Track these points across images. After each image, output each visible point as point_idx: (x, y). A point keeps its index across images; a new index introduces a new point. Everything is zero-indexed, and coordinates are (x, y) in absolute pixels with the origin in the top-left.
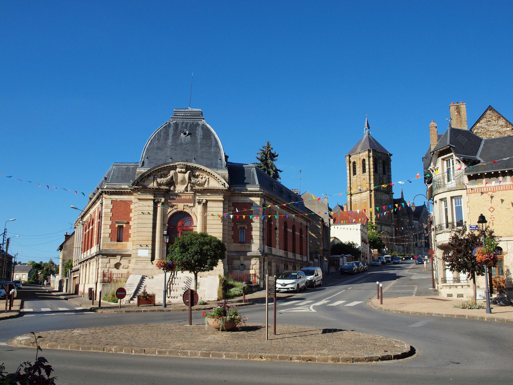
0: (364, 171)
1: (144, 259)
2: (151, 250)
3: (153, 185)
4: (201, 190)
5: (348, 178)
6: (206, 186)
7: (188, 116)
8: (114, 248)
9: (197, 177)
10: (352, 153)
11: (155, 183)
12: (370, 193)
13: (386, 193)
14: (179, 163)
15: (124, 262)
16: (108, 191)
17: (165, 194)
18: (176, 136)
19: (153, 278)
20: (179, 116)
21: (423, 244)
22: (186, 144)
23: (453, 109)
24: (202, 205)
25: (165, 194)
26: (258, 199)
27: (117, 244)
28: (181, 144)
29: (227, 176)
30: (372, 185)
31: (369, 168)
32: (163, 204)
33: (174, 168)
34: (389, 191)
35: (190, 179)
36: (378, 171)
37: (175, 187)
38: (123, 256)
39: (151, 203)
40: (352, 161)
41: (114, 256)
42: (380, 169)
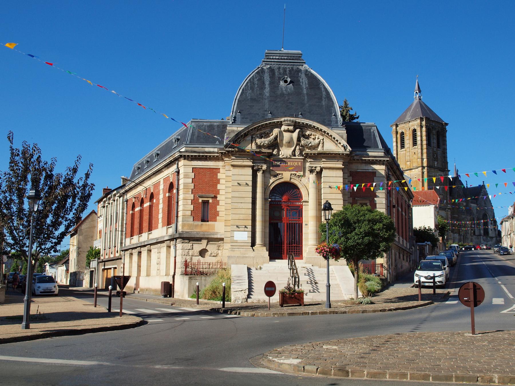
0: (415, 143)
1: (243, 244)
2: (251, 232)
3: (251, 147)
4: (314, 154)
6: (320, 149)
7: (284, 59)
8: (198, 230)
9: (308, 137)
10: (400, 121)
11: (253, 144)
12: (422, 169)
13: (440, 170)
14: (286, 118)
15: (212, 248)
16: (188, 156)
17: (266, 160)
18: (274, 85)
19: (261, 268)
20: (273, 59)
21: (482, 232)
22: (289, 94)
24: (315, 173)
25: (266, 160)
26: (383, 167)
27: (202, 225)
28: (282, 95)
29: (345, 136)
30: (425, 160)
31: (422, 140)
32: (264, 172)
33: (279, 125)
34: (444, 169)
35: (299, 140)
36: (432, 144)
37: (279, 151)
38: (210, 240)
39: (250, 171)
40: (400, 131)
41: (199, 240)
42: (434, 141)
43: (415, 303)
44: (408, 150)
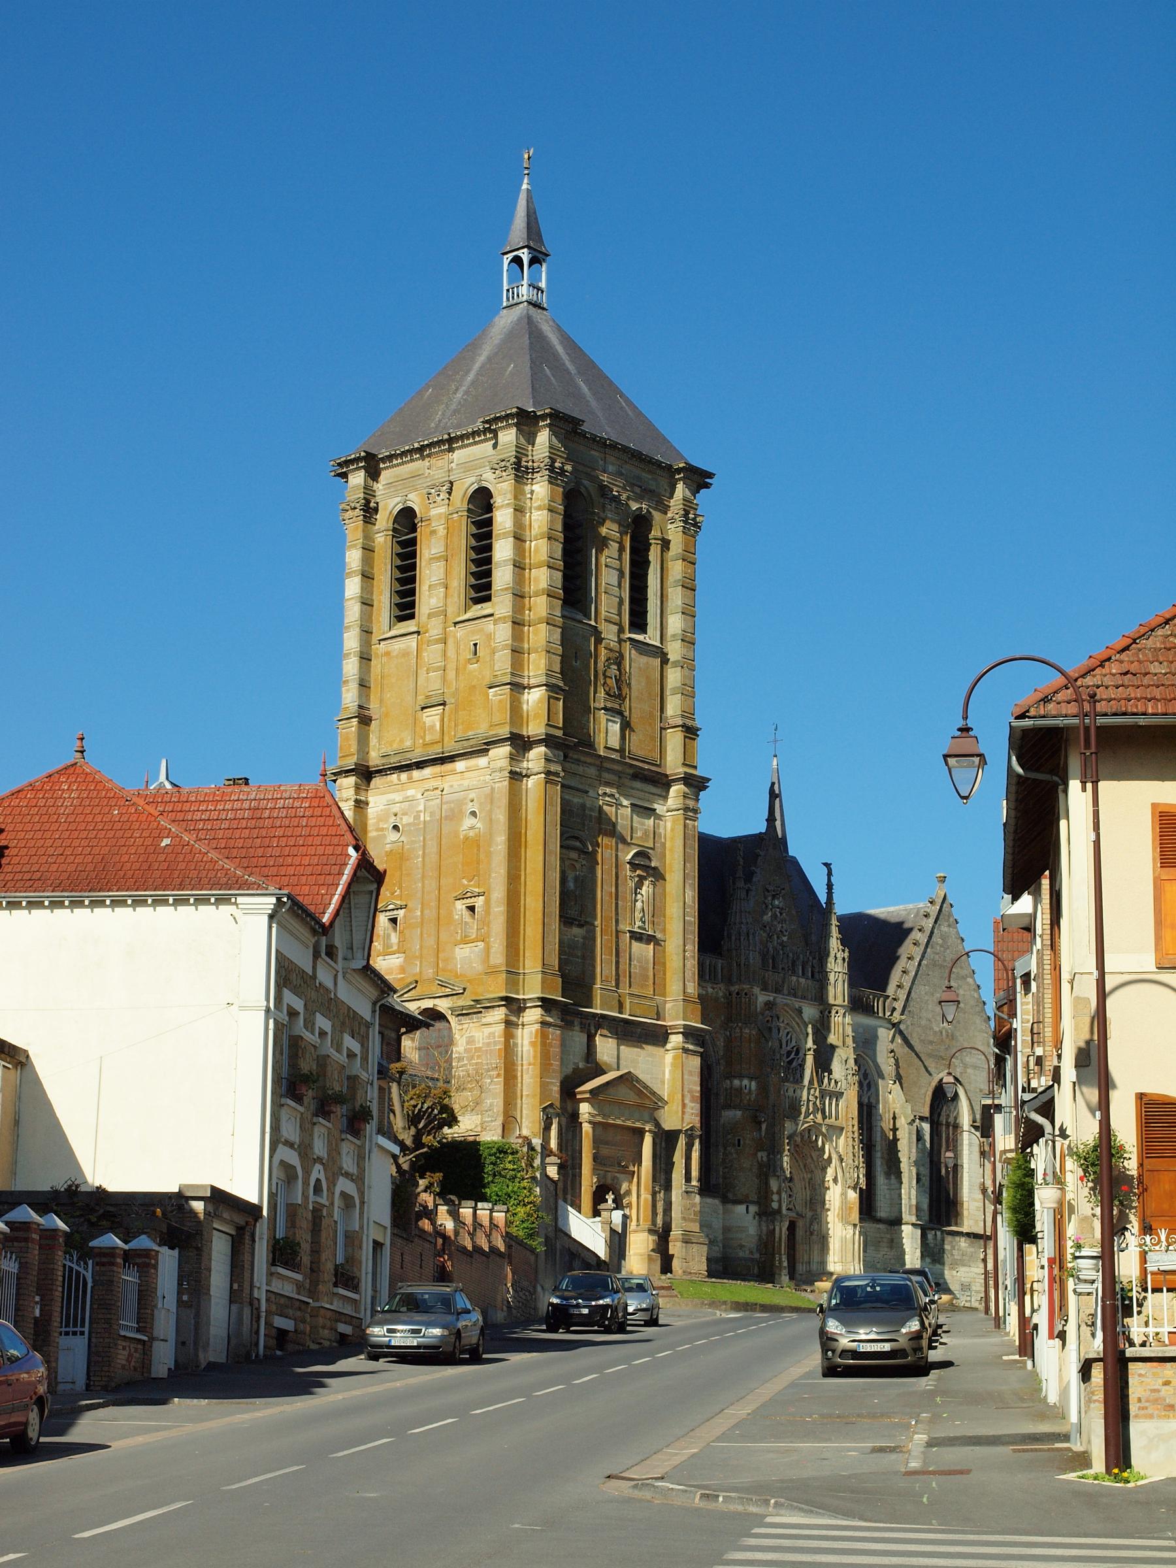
0: (481, 589)
5: (351, 641)
23: (576, 1311)
43: (660, 1210)
44: (434, 629)
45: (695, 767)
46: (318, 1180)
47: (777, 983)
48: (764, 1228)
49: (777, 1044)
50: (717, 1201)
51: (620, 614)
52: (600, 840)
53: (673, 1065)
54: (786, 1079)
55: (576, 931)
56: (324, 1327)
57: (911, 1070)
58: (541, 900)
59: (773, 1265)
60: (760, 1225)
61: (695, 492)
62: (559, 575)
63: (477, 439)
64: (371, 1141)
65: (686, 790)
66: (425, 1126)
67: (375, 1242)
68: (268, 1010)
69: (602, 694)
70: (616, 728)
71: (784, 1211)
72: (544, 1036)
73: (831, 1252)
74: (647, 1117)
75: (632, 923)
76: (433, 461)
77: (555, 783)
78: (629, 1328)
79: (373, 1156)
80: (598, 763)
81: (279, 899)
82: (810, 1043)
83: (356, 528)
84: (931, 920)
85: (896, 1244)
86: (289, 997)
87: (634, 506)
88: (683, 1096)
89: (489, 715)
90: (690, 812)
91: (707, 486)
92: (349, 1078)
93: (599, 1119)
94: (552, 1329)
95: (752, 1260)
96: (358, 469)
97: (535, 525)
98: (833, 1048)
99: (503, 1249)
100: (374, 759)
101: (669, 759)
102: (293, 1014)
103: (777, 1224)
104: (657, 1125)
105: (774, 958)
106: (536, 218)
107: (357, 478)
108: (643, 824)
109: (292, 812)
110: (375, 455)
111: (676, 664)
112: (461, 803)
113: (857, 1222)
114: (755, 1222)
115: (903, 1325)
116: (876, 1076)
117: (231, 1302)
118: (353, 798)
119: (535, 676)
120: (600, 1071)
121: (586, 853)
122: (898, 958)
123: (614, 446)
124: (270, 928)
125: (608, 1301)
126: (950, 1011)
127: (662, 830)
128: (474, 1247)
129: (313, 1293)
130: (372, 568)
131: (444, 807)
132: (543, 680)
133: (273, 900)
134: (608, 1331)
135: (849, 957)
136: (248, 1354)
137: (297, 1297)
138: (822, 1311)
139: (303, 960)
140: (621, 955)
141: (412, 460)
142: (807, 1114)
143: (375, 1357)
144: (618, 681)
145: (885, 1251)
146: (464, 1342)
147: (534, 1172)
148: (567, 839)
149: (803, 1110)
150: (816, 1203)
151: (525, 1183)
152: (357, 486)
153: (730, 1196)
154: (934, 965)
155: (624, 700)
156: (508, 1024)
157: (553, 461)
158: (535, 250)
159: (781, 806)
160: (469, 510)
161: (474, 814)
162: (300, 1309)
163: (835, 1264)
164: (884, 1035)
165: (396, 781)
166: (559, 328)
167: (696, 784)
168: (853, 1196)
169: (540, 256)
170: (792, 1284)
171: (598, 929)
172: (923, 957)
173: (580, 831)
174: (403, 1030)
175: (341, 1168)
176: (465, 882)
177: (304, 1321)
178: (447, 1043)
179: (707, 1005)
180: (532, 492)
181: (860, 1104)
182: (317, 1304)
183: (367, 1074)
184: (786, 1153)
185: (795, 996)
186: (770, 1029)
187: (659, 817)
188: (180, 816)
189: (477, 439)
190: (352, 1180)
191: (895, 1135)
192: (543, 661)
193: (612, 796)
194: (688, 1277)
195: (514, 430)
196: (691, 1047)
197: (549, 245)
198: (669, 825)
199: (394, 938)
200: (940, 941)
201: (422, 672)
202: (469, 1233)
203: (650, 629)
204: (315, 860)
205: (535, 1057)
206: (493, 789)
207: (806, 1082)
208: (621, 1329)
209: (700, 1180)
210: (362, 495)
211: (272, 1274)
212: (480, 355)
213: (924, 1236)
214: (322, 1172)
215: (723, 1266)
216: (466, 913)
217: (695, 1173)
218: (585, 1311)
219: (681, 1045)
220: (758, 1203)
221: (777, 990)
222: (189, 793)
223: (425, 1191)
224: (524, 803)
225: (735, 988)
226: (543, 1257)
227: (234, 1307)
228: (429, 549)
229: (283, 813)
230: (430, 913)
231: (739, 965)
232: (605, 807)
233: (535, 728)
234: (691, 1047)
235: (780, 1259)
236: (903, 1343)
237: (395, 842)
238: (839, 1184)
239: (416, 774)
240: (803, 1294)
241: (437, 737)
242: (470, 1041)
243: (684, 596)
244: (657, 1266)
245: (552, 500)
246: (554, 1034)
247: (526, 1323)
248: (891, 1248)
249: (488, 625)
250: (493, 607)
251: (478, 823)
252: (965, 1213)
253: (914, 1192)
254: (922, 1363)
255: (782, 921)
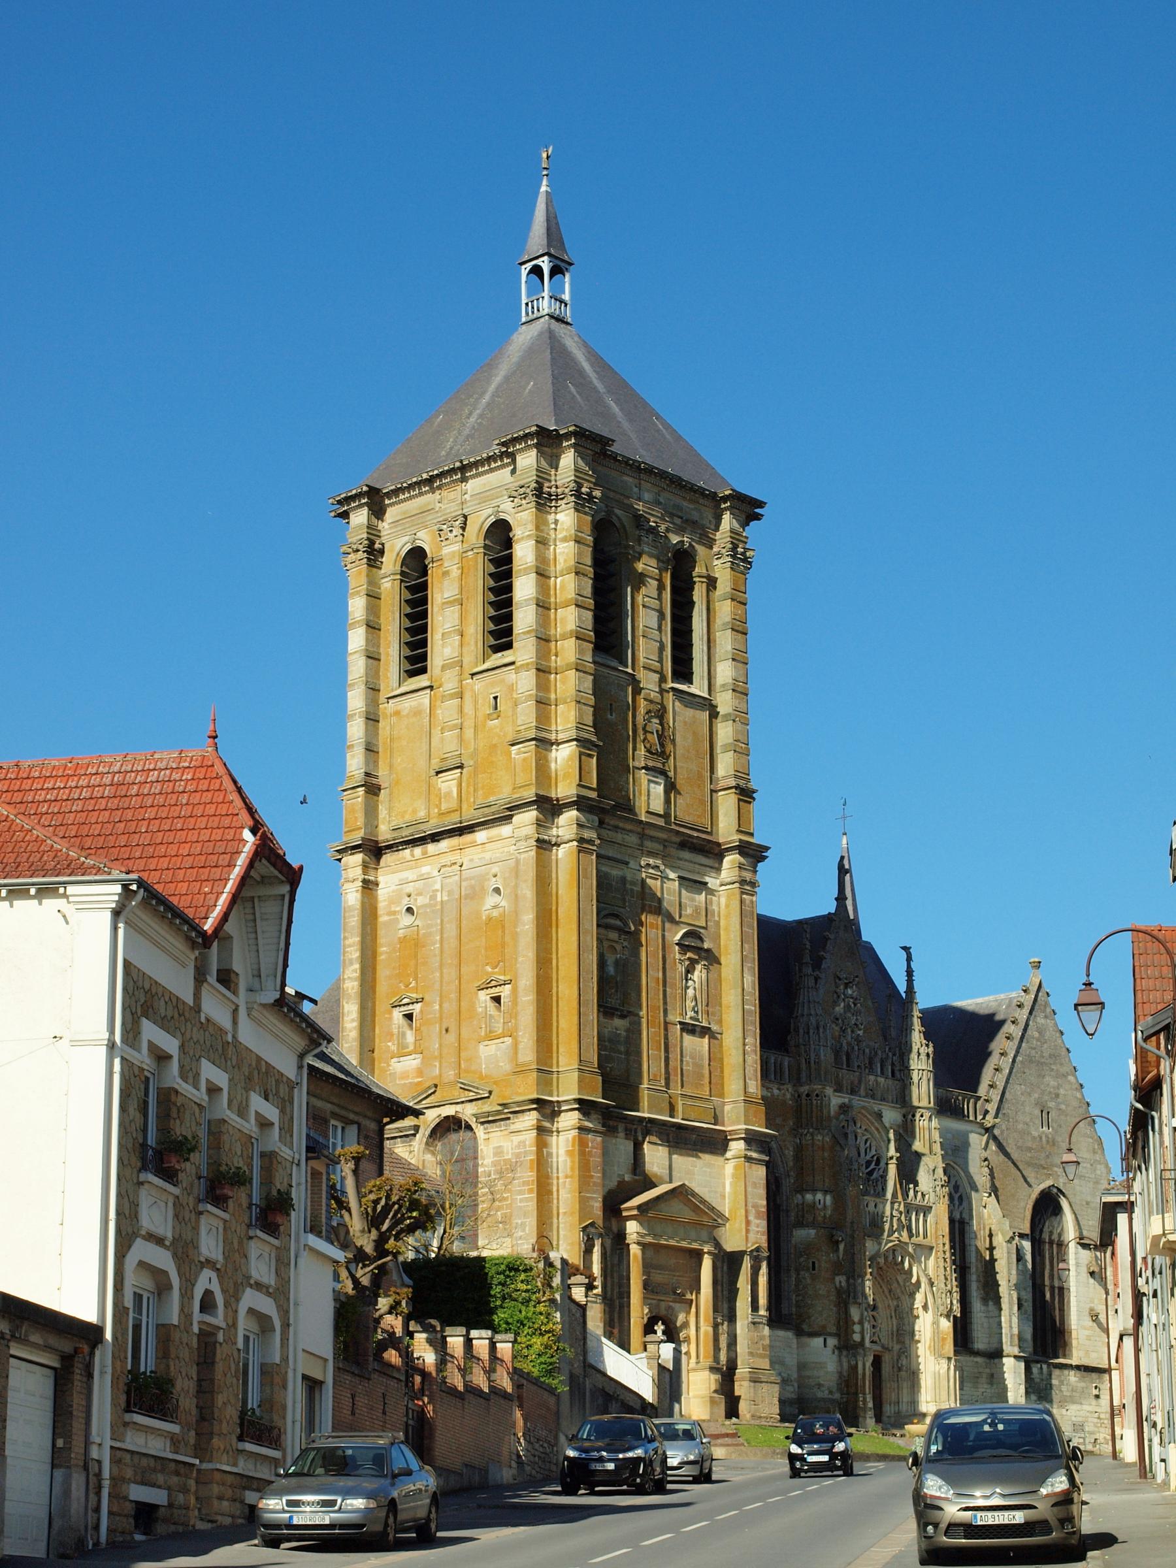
0: (501, 635)
5: (356, 700)
23: (599, 1467)
40: (396, 546)
44: (449, 682)
45: (752, 835)
46: (208, 1294)
47: (852, 1083)
48: (845, 1365)
49: (854, 1153)
50: (790, 1334)
51: (661, 661)
52: (643, 918)
53: (734, 1176)
54: (865, 1193)
55: (618, 1022)
56: (220, 1498)
57: (1009, 1181)
58: (576, 987)
59: (856, 1407)
60: (840, 1361)
61: (745, 524)
62: (589, 616)
63: (493, 465)
64: (297, 1241)
65: (742, 860)
66: (390, 1229)
67: (305, 1377)
68: (111, 1046)
69: (641, 751)
70: (659, 790)
71: (867, 1344)
72: (582, 1144)
73: (923, 1390)
74: (704, 1235)
75: (683, 1013)
76: (445, 493)
77: (590, 852)
78: (669, 1486)
79: (301, 1261)
80: (639, 830)
81: (125, 887)
82: (892, 1151)
83: (360, 573)
84: (1026, 1011)
85: (996, 1380)
86: (150, 1031)
87: (675, 539)
88: (746, 1211)
89: (513, 777)
90: (747, 886)
91: (758, 517)
92: (263, 1155)
93: (649, 1239)
94: (570, 1491)
95: (833, 1400)
96: (361, 506)
97: (561, 559)
98: (918, 1156)
99: (509, 1390)
100: (384, 833)
101: (721, 825)
102: (162, 1058)
103: (860, 1359)
104: (717, 1245)
105: (848, 1055)
106: (557, 224)
107: (360, 517)
108: (693, 900)
109: (168, 787)
110: (378, 491)
111: (727, 717)
112: (482, 879)
113: (951, 1354)
114: (835, 1357)
115: (1042, 1482)
116: (968, 1190)
117: (53, 1466)
118: (361, 877)
119: (565, 730)
120: (650, 1184)
121: (629, 933)
122: (990, 1054)
123: (650, 471)
124: (115, 929)
125: (639, 1452)
126: (1090, 1015)
127: (715, 907)
128: (465, 1386)
129: (202, 1450)
130: (379, 617)
131: (464, 884)
132: (573, 734)
133: (118, 888)
134: (640, 1491)
135: (935, 1052)
136: (81, 1542)
137: (171, 1456)
138: (916, 1462)
139: (176, 980)
140: (671, 1049)
141: (421, 494)
142: (891, 1232)
143: (273, 1542)
144: (660, 737)
145: (984, 1387)
146: (401, 1517)
147: (553, 1293)
148: (606, 916)
149: (887, 1226)
150: (904, 1334)
151: (541, 1308)
152: (360, 526)
153: (805, 1327)
154: (1031, 1061)
155: (668, 758)
156: (541, 1130)
157: (580, 486)
158: (557, 258)
159: (852, 883)
160: (486, 547)
161: (497, 891)
162: (177, 1474)
163: (929, 1403)
164: (977, 1141)
165: (409, 857)
166: (586, 345)
167: (754, 853)
168: (946, 1325)
169: (562, 265)
170: (879, 1427)
171: (644, 1021)
172: (1017, 1052)
173: (619, 910)
174: (386, 1120)
175: (249, 1277)
176: (489, 969)
177: (185, 1490)
178: (470, 1156)
179: (772, 1109)
180: (556, 522)
181: (952, 1221)
182: (210, 1466)
183: (293, 1150)
184: (868, 1276)
185: (873, 1097)
186: (846, 1135)
187: (711, 892)
188: (18, 797)
189: (493, 465)
190: (269, 1294)
191: (991, 1255)
192: (573, 713)
193: (656, 867)
194: (757, 1422)
195: (533, 453)
196: (755, 1155)
197: (571, 254)
198: (723, 900)
199: (410, 1037)
200: (1036, 1035)
201: (436, 732)
202: (459, 1369)
203: (696, 678)
204: (197, 849)
205: (572, 1169)
206: (518, 861)
207: (889, 1195)
208: (659, 1487)
209: (769, 1309)
210: (365, 536)
211: (126, 1424)
212: (496, 376)
213: (1028, 1370)
214: (215, 1280)
215: (797, 1408)
216: (491, 1005)
217: (763, 1300)
218: (611, 1466)
219: (743, 1153)
220: (837, 1335)
221: (853, 1091)
222: (31, 768)
223: (390, 1313)
224: (554, 876)
225: (804, 1089)
226: (566, 1399)
227: (58, 1473)
228: (442, 593)
229: (157, 788)
230: (450, 1007)
231: (808, 1062)
232: (648, 881)
233: (565, 789)
234: (755, 1155)
235: (865, 1399)
236: (1043, 1510)
237: (408, 927)
238: (930, 1312)
239: (431, 848)
240: (892, 1439)
241: (454, 804)
242: (498, 1151)
243: (734, 640)
244: (721, 1410)
245: (579, 530)
246: (594, 1141)
247: (535, 1484)
248: (991, 1384)
249: (509, 675)
250: (514, 654)
251: (503, 902)
252: (1074, 1343)
253: (1015, 1320)
254: (1074, 1541)
255: (857, 1013)
